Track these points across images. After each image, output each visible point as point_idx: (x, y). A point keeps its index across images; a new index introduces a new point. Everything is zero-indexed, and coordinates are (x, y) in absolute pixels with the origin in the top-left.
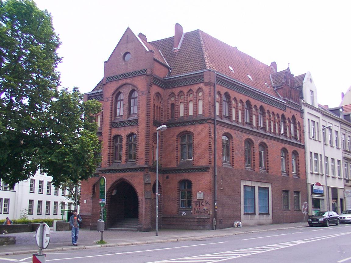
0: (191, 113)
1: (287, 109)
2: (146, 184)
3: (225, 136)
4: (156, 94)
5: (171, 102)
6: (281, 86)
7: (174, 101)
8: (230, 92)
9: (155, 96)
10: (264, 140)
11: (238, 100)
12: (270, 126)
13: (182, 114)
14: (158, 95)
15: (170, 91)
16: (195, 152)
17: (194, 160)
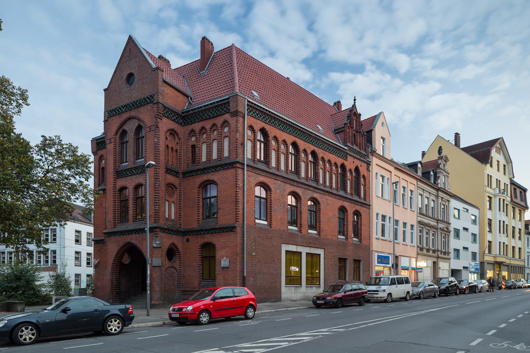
0: (215, 156)
1: (349, 157)
2: (203, 257)
3: (261, 186)
4: (170, 132)
5: (191, 143)
6: (343, 127)
7: (194, 141)
8: (268, 128)
9: (168, 134)
10: (316, 195)
11: (280, 140)
12: (324, 177)
13: (204, 159)
14: (173, 133)
15: (190, 127)
16: (219, 207)
17: (218, 217)
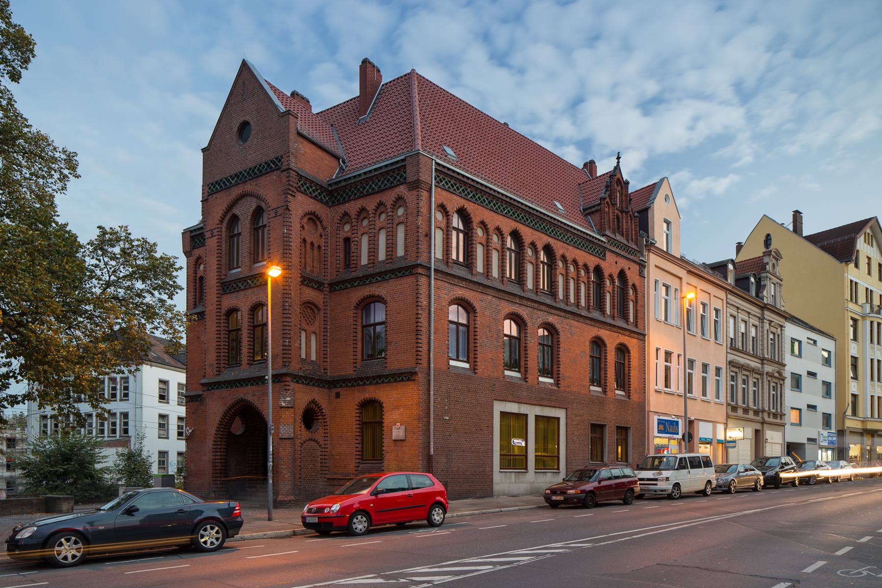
0: (382, 256)
3: (458, 305)
4: (308, 217)
5: (343, 235)
8: (470, 207)
9: (306, 220)
10: (551, 319)
11: (491, 227)
13: (364, 261)
14: (313, 218)
17: (388, 357)
